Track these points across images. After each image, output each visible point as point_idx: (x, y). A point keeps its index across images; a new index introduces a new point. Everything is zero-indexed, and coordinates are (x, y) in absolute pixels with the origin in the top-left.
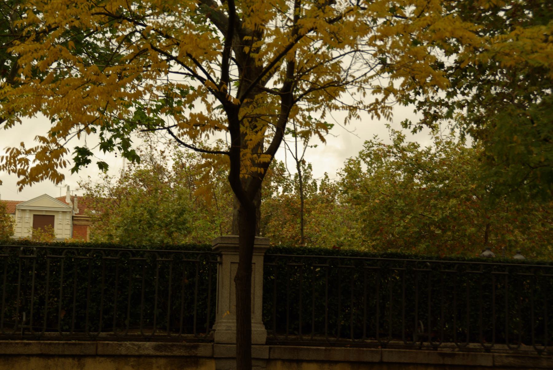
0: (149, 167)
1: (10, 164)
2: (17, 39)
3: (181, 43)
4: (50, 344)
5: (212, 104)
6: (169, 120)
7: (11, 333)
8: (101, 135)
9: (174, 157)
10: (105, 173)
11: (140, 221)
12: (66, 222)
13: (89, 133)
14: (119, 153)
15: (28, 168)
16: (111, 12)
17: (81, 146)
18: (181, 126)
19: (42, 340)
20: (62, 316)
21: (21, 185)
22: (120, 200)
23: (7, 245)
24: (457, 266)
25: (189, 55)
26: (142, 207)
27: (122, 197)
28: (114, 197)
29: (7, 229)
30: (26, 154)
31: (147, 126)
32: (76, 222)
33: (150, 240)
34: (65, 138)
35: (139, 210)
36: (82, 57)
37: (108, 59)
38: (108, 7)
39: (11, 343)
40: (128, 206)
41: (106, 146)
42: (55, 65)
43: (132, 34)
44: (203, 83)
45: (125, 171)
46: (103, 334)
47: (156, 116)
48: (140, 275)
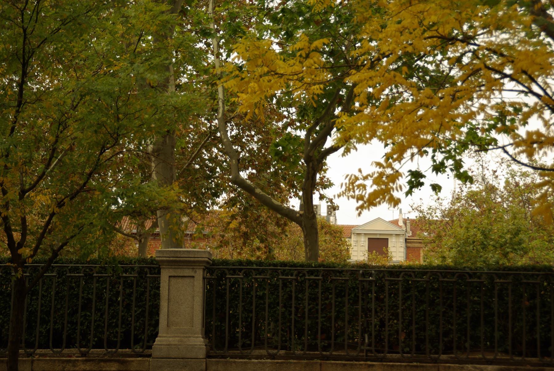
0: (481, 187)
1: (349, 190)
2: (353, 69)
3: (515, 60)
4: (393, 366)
5: (549, 121)
6: (503, 139)
7: (355, 354)
8: (433, 157)
9: (506, 176)
10: (437, 194)
11: (474, 242)
12: (399, 245)
13: (422, 156)
14: (452, 174)
15: (366, 193)
16: (443, 34)
17: (413, 170)
18: (517, 145)
19: (385, 362)
20: (402, 337)
21: (360, 210)
22: (453, 221)
23: (347, 268)
24: (56, 269)
25: (525, 72)
26: (475, 228)
27: (455, 218)
28: (446, 219)
29: (344, 253)
30: (364, 180)
31: (480, 146)
32: (409, 245)
33: (484, 262)
34: (400, 162)
35: (472, 232)
36: (414, 80)
37: (439, 81)
38: (440, 30)
39: (356, 365)
40: (461, 227)
41: (439, 168)
42: (387, 91)
43: (463, 55)
44: (540, 99)
45: (457, 192)
46: (444, 357)
47: (488, 136)
48: (478, 297)
